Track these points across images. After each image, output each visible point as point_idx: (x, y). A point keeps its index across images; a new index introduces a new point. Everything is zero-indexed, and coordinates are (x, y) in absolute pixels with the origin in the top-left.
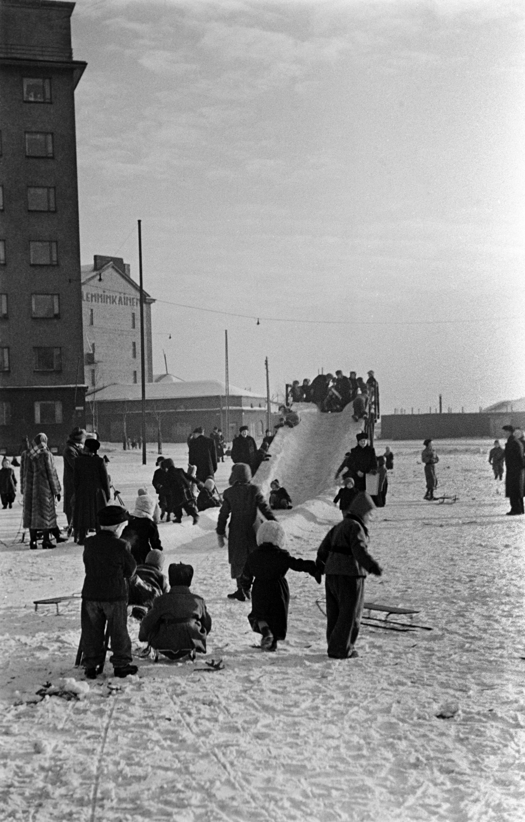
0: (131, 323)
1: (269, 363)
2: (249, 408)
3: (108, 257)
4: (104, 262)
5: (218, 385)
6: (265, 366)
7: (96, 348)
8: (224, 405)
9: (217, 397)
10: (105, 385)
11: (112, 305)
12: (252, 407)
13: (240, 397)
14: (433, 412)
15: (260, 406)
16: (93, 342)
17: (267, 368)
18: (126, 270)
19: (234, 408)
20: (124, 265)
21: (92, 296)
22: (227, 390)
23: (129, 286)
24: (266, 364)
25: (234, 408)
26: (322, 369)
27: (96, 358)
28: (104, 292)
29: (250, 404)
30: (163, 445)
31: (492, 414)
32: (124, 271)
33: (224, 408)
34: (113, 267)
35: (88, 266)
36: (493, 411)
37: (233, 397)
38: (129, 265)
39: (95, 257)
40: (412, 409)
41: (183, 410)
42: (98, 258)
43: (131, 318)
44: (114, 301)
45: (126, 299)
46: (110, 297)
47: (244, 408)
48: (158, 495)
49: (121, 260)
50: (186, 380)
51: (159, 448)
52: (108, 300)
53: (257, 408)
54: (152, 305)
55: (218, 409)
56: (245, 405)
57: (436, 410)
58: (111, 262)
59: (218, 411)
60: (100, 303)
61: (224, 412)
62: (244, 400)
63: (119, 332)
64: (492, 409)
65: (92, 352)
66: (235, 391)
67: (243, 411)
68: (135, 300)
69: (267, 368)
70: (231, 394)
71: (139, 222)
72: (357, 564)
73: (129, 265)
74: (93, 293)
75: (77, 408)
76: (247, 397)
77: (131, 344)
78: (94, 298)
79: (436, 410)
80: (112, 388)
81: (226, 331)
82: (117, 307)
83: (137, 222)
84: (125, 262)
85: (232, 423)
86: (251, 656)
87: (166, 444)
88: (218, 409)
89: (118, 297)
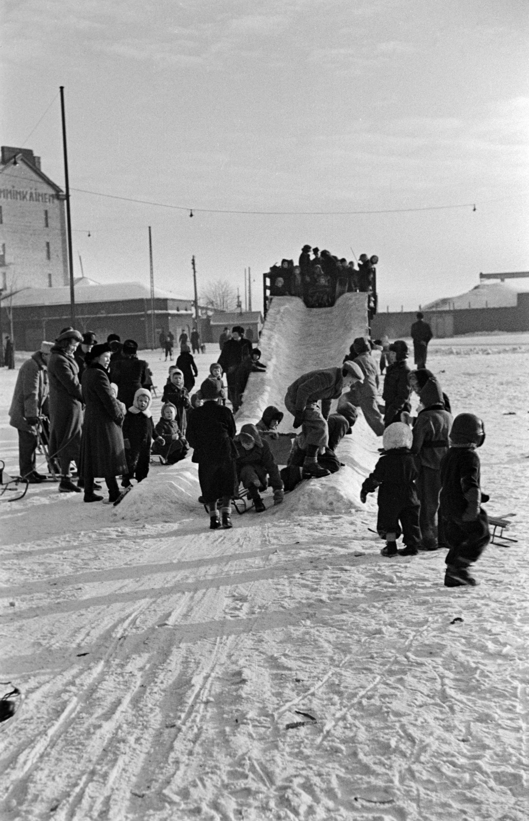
0: (43, 222)
1: (196, 262)
2: (175, 312)
3: (17, 149)
5: (141, 287)
6: (191, 266)
8: (148, 310)
9: (141, 300)
12: (178, 310)
13: (165, 300)
15: (186, 310)
17: (194, 268)
18: (37, 164)
19: (160, 312)
20: (34, 157)
22: (152, 291)
24: (193, 263)
25: (160, 312)
26: (249, 268)
28: (13, 187)
29: (175, 307)
31: (433, 312)
32: (34, 165)
33: (149, 312)
36: (434, 309)
37: (159, 300)
40: (402, 307)
42: (5, 149)
43: (44, 216)
44: (24, 197)
46: (20, 193)
47: (170, 312)
48: (196, 466)
52: (18, 196)
53: (183, 312)
55: (143, 313)
56: (172, 309)
58: (20, 155)
59: (142, 316)
60: (9, 199)
61: (149, 316)
62: (170, 303)
64: (433, 307)
66: (161, 293)
67: (169, 315)
68: (47, 196)
69: (194, 268)
70: (157, 296)
71: (62, 88)
72: (80, 388)
76: (173, 300)
77: (44, 245)
81: (150, 228)
82: (27, 204)
83: (59, 90)
84: (36, 154)
85: (158, 328)
86: (428, 795)
88: (143, 313)
89: (29, 192)
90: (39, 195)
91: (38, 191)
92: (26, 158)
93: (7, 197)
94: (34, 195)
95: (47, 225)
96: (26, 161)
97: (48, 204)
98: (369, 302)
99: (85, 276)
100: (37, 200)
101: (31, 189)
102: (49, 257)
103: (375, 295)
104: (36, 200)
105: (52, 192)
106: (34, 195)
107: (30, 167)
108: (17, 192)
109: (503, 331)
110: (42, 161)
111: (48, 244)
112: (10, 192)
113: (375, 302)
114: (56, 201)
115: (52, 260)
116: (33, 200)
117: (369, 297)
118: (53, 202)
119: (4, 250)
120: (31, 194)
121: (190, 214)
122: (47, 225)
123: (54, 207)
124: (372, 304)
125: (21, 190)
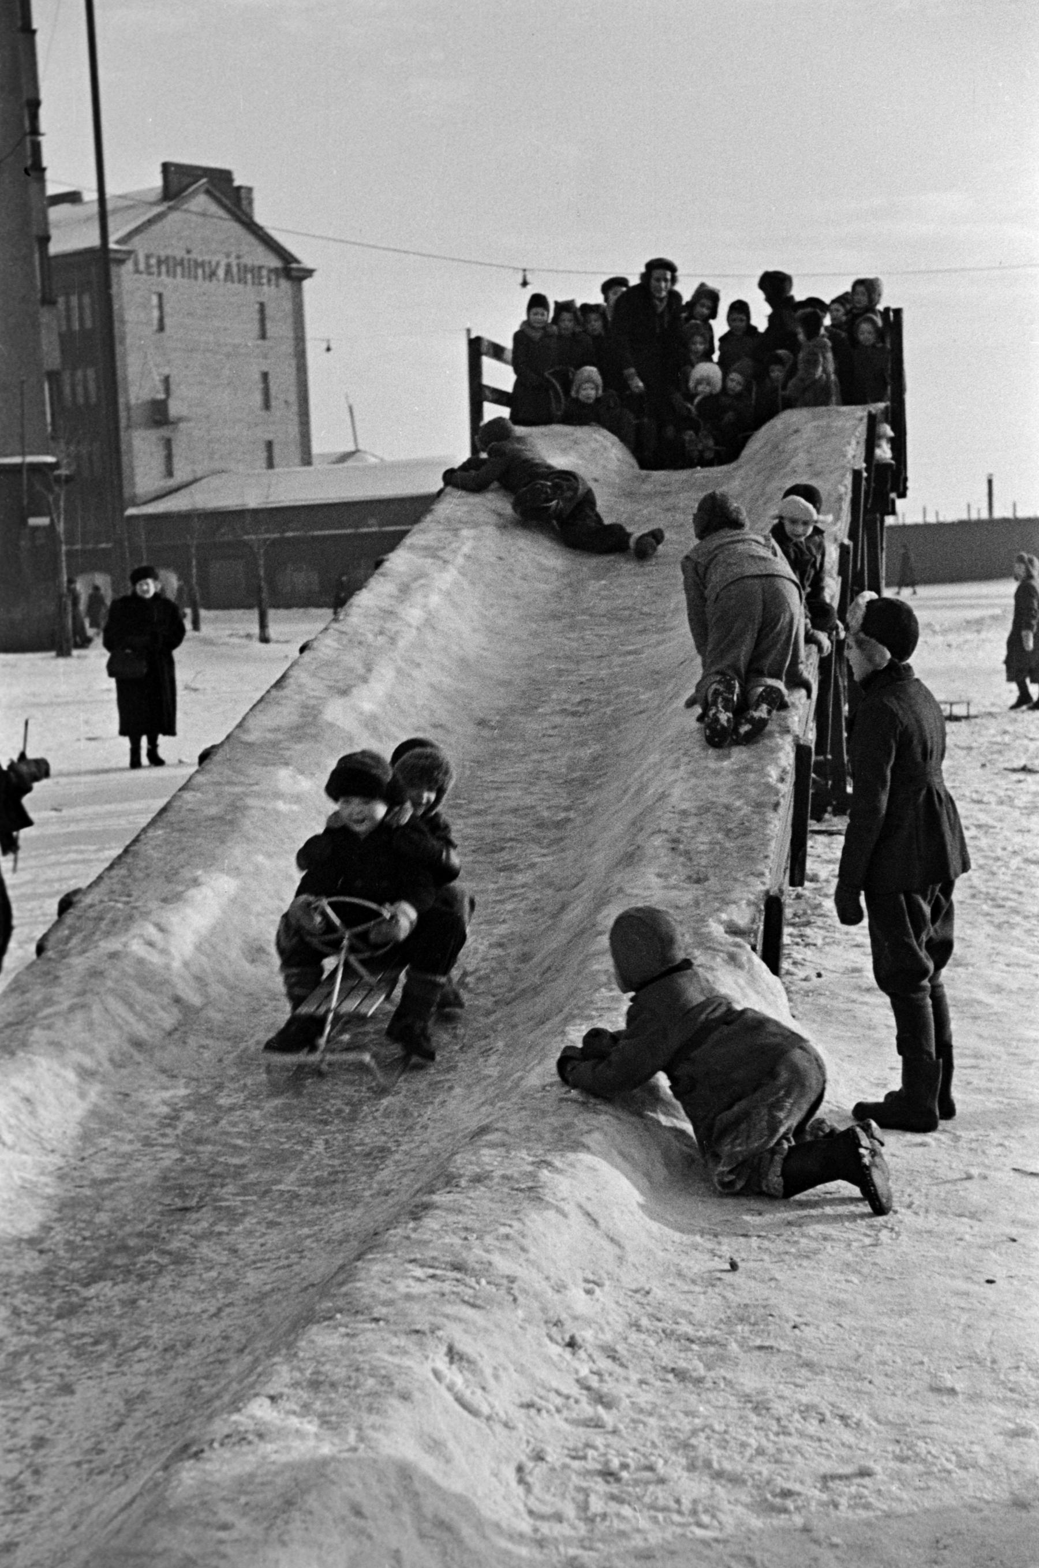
4: (186, 180)
7: (173, 387)
10: (199, 474)
11: (207, 283)
14: (974, 516)
16: (166, 371)
18: (244, 202)
21: (160, 262)
23: (251, 239)
27: (174, 409)
28: (189, 252)
30: (272, 613)
34: (208, 192)
35: (151, 190)
38: (250, 190)
39: (166, 167)
41: (374, 529)
43: (257, 316)
44: (213, 274)
45: (244, 269)
46: (202, 265)
49: (225, 176)
50: (388, 458)
51: (263, 625)
52: (200, 272)
54: (307, 284)
57: (979, 511)
58: (204, 180)
63: (229, 349)
65: (162, 396)
68: (264, 273)
73: (250, 190)
74: (163, 254)
75: (33, 521)
77: (257, 377)
78: (164, 269)
79: (979, 511)
80: (215, 482)
82: (220, 290)
87: (282, 612)
89: (223, 263)
90: (246, 271)
91: (243, 261)
92: (214, 186)
93: (175, 276)
94: (235, 270)
95: (263, 336)
96: (218, 194)
97: (265, 288)
98: (871, 442)
99: (361, 447)
100: (242, 280)
101: (228, 255)
102: (267, 405)
103: (897, 417)
104: (240, 281)
105: (275, 263)
106: (235, 270)
107: (228, 210)
108: (196, 261)
109: (288, 606)
110: (256, 196)
111: (265, 376)
112: (181, 263)
113: (899, 445)
114: (285, 284)
115: (273, 410)
116: (233, 282)
117: (872, 421)
118: (277, 286)
119: (167, 390)
120: (228, 266)
121: (520, 280)
122: (263, 336)
123: (275, 294)
124: (884, 452)
125: (207, 258)
